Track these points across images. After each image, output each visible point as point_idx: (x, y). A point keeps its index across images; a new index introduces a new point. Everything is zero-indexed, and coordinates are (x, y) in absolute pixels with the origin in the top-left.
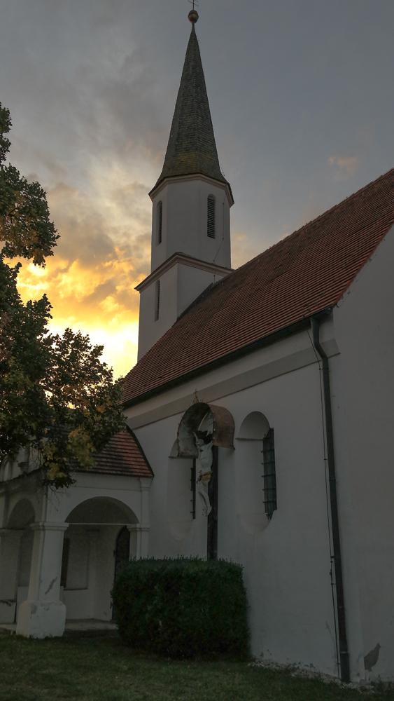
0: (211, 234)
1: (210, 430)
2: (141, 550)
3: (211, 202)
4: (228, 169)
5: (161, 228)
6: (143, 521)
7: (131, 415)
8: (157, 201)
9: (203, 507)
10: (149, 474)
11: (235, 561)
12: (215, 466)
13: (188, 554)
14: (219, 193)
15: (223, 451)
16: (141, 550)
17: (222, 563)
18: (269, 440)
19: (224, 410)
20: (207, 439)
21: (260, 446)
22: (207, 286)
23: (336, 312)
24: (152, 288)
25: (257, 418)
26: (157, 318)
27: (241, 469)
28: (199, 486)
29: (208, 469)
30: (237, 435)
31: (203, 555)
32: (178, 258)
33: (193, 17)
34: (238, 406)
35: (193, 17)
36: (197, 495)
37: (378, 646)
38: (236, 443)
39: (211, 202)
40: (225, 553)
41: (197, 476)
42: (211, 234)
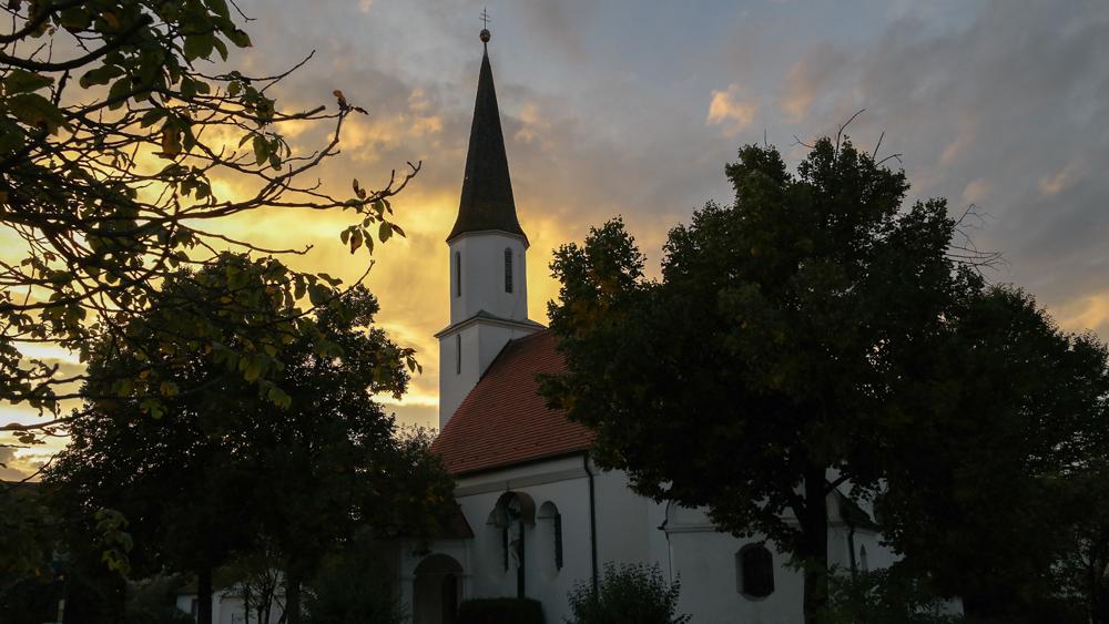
0: (509, 289)
1: (518, 509)
2: (468, 592)
3: (508, 254)
4: (527, 227)
5: (459, 265)
6: (468, 571)
7: (462, 485)
8: (456, 250)
9: (513, 562)
10: (470, 534)
11: (537, 598)
12: (522, 535)
13: (505, 594)
14: (512, 243)
15: (527, 527)
16: (468, 592)
17: (529, 600)
18: (558, 518)
19: (528, 496)
20: (516, 516)
21: (553, 520)
22: (505, 343)
23: (560, 512)
24: (452, 340)
25: (549, 505)
26: (459, 372)
27: (539, 540)
28: (510, 549)
29: (517, 538)
30: (538, 513)
31: (515, 594)
32: (482, 317)
33: (485, 36)
34: (539, 494)
35: (485, 36)
36: (510, 555)
37: (352, 252)
38: (536, 521)
39: (508, 254)
40: (530, 593)
41: (509, 541)
42: (509, 289)
